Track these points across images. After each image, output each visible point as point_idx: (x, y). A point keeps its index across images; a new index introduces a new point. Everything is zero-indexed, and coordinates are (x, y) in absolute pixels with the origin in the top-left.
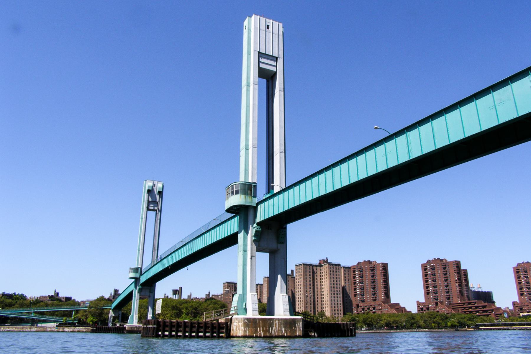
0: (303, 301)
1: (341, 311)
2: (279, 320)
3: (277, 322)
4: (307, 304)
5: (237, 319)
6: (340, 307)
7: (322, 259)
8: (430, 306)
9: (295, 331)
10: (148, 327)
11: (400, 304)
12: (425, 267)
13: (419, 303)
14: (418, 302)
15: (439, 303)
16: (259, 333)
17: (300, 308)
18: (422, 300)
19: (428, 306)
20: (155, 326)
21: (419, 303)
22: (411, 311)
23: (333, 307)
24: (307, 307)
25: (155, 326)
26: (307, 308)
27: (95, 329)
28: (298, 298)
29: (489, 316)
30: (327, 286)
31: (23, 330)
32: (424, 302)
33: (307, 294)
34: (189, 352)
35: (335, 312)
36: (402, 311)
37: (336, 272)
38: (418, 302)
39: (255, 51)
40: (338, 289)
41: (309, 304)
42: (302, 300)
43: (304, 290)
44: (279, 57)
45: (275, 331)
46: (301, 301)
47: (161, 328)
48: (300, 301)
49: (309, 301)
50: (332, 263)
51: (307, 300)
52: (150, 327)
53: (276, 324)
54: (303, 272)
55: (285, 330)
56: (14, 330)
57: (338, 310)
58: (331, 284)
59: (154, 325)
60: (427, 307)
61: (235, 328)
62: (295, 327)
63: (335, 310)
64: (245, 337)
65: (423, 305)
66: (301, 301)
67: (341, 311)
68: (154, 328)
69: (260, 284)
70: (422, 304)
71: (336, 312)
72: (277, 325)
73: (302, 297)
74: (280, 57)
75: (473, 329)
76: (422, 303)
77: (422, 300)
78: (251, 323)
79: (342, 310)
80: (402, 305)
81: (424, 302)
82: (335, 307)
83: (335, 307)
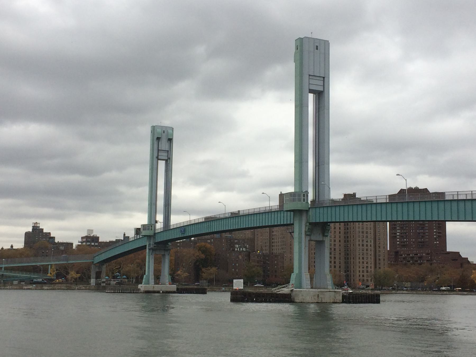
11: (460, 253)
22: (50, 233)
63: (363, 262)
68: (242, 297)
82: (363, 258)
83: (363, 258)
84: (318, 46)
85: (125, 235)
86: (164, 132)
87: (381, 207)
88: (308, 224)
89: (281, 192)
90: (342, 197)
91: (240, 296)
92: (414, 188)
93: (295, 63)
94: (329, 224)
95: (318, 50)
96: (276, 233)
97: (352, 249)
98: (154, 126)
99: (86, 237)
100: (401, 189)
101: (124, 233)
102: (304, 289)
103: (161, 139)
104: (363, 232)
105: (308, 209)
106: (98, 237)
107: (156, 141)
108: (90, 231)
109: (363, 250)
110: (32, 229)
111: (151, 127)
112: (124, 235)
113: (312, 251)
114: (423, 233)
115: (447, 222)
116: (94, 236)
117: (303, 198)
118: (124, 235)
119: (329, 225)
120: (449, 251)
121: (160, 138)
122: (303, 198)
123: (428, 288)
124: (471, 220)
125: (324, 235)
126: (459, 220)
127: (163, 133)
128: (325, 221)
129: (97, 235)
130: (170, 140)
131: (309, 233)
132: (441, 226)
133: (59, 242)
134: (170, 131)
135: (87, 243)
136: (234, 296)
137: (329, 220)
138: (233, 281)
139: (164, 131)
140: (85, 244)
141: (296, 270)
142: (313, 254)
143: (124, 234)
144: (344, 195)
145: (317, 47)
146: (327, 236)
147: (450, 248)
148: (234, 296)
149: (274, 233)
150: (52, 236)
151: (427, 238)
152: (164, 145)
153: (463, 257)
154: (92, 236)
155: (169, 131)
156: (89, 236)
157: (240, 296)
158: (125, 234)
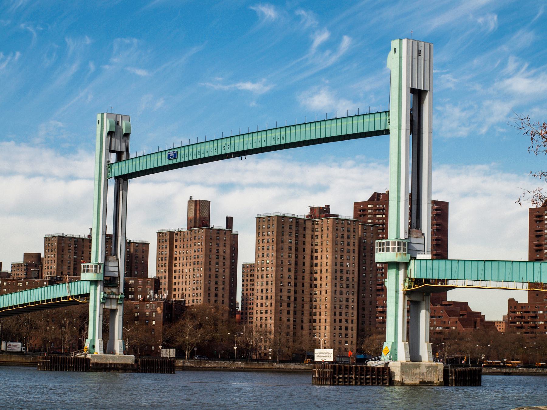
0: (273, 297)
1: (352, 322)
4: (281, 306)
6: (352, 313)
7: (316, 205)
8: (541, 312)
11: (469, 305)
12: (537, 231)
17: (264, 312)
19: (535, 312)
20: (332, 370)
22: (481, 313)
23: (338, 314)
25: (332, 370)
26: (281, 313)
27: (49, 360)
28: (259, 291)
30: (327, 268)
32: (527, 302)
33: (281, 282)
34: (145, 405)
35: (341, 324)
36: (475, 323)
37: (349, 237)
39: (407, 87)
40: (351, 276)
41: (285, 305)
42: (271, 296)
43: (276, 275)
44: (429, 91)
46: (269, 297)
47: (337, 372)
48: (264, 297)
49: (285, 298)
50: (340, 217)
51: (281, 297)
52: (326, 371)
54: (275, 234)
57: (347, 321)
58: (336, 265)
60: (532, 314)
63: (340, 321)
65: (524, 309)
66: (269, 297)
67: (352, 322)
68: (331, 371)
69: (135, 241)
70: (522, 308)
71: (344, 324)
73: (352, 313)
74: (431, 90)
76: (522, 306)
79: (355, 321)
80: (474, 307)
81: (527, 302)
82: (341, 314)
83: (341, 314)
89: (191, 198)
90: (307, 212)
91: (329, 370)
96: (181, 268)
97: (323, 298)
100: (375, 193)
103: (114, 134)
104: (341, 271)
109: (341, 301)
113: (258, 300)
117: (403, 247)
120: (451, 301)
122: (403, 247)
123: (336, 374)
136: (320, 370)
138: (314, 350)
141: (90, 337)
142: (259, 305)
144: (311, 208)
148: (320, 370)
149: (177, 268)
150: (482, 314)
153: (473, 310)
157: (329, 370)
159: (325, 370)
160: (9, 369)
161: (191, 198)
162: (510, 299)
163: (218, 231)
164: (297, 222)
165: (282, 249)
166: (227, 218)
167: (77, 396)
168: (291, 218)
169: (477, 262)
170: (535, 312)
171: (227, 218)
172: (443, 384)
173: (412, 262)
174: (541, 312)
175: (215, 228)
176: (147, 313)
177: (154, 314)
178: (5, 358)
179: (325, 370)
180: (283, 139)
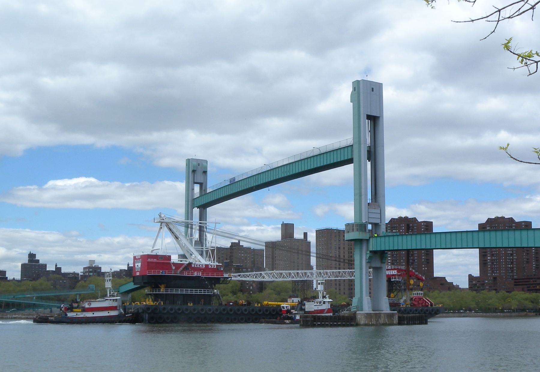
2: (384, 313)
3: (383, 315)
5: (360, 313)
8: (487, 281)
9: (393, 320)
10: (307, 320)
13: (471, 277)
14: (470, 276)
15: (498, 278)
16: (373, 322)
18: (476, 273)
19: (483, 281)
20: (312, 319)
21: (471, 277)
24: (331, 284)
25: (312, 319)
29: (439, 351)
31: (31, 317)
32: (479, 276)
38: (470, 276)
45: (381, 321)
53: (382, 316)
55: (388, 320)
56: (22, 317)
59: (312, 318)
60: (481, 283)
61: (359, 319)
62: (393, 318)
64: (366, 325)
72: (383, 316)
75: (535, 314)
77: (476, 273)
78: (368, 316)
84: (373, 88)
85: (57, 266)
86: (199, 165)
87: (407, 237)
88: (368, 252)
89: (283, 222)
92: (404, 217)
93: (352, 103)
94: (386, 252)
95: (373, 91)
98: (190, 159)
99: (89, 268)
101: (128, 264)
102: (365, 311)
103: (196, 171)
105: (368, 238)
106: (100, 267)
107: (192, 173)
108: (92, 262)
110: (28, 260)
111: (186, 160)
112: (128, 265)
114: (413, 260)
115: (434, 250)
116: (96, 266)
118: (56, 265)
119: (387, 253)
121: (196, 170)
124: (461, 247)
125: (382, 262)
126: (452, 247)
127: (198, 165)
128: (383, 249)
129: (98, 265)
130: (205, 172)
131: (370, 260)
132: (429, 254)
133: (75, 272)
134: (205, 164)
135: (90, 273)
137: (414, 247)
139: (199, 164)
140: (87, 274)
143: (128, 264)
145: (373, 89)
146: (384, 263)
147: (437, 274)
151: (416, 265)
152: (199, 178)
154: (94, 266)
155: (204, 164)
156: (91, 266)
158: (57, 264)
159: (307, 319)
160: (191, 330)
161: (283, 222)
162: (471, 275)
163: (298, 240)
164: (339, 232)
165: (331, 248)
166: (304, 233)
167: (413, 366)
168: (335, 230)
169: (275, 170)
170: (483, 281)
171: (304, 233)
172: (56, 267)
173: (371, 240)
174: (487, 281)
175: (296, 238)
176: (247, 287)
177: (251, 287)
178: (4, 299)
179: (307, 319)
180: (288, 172)
